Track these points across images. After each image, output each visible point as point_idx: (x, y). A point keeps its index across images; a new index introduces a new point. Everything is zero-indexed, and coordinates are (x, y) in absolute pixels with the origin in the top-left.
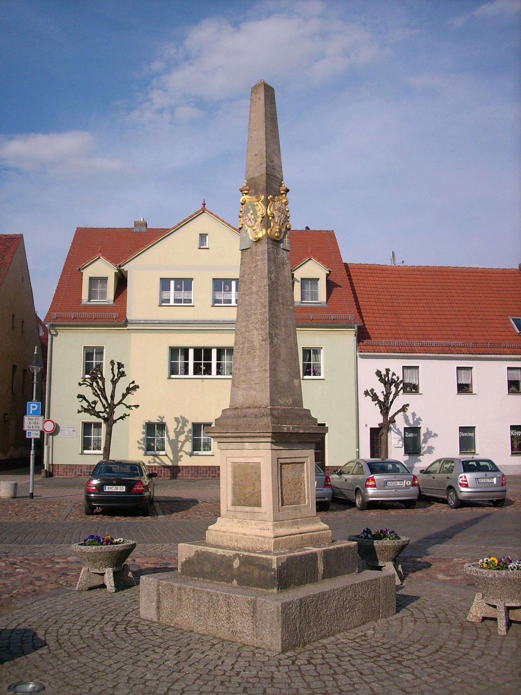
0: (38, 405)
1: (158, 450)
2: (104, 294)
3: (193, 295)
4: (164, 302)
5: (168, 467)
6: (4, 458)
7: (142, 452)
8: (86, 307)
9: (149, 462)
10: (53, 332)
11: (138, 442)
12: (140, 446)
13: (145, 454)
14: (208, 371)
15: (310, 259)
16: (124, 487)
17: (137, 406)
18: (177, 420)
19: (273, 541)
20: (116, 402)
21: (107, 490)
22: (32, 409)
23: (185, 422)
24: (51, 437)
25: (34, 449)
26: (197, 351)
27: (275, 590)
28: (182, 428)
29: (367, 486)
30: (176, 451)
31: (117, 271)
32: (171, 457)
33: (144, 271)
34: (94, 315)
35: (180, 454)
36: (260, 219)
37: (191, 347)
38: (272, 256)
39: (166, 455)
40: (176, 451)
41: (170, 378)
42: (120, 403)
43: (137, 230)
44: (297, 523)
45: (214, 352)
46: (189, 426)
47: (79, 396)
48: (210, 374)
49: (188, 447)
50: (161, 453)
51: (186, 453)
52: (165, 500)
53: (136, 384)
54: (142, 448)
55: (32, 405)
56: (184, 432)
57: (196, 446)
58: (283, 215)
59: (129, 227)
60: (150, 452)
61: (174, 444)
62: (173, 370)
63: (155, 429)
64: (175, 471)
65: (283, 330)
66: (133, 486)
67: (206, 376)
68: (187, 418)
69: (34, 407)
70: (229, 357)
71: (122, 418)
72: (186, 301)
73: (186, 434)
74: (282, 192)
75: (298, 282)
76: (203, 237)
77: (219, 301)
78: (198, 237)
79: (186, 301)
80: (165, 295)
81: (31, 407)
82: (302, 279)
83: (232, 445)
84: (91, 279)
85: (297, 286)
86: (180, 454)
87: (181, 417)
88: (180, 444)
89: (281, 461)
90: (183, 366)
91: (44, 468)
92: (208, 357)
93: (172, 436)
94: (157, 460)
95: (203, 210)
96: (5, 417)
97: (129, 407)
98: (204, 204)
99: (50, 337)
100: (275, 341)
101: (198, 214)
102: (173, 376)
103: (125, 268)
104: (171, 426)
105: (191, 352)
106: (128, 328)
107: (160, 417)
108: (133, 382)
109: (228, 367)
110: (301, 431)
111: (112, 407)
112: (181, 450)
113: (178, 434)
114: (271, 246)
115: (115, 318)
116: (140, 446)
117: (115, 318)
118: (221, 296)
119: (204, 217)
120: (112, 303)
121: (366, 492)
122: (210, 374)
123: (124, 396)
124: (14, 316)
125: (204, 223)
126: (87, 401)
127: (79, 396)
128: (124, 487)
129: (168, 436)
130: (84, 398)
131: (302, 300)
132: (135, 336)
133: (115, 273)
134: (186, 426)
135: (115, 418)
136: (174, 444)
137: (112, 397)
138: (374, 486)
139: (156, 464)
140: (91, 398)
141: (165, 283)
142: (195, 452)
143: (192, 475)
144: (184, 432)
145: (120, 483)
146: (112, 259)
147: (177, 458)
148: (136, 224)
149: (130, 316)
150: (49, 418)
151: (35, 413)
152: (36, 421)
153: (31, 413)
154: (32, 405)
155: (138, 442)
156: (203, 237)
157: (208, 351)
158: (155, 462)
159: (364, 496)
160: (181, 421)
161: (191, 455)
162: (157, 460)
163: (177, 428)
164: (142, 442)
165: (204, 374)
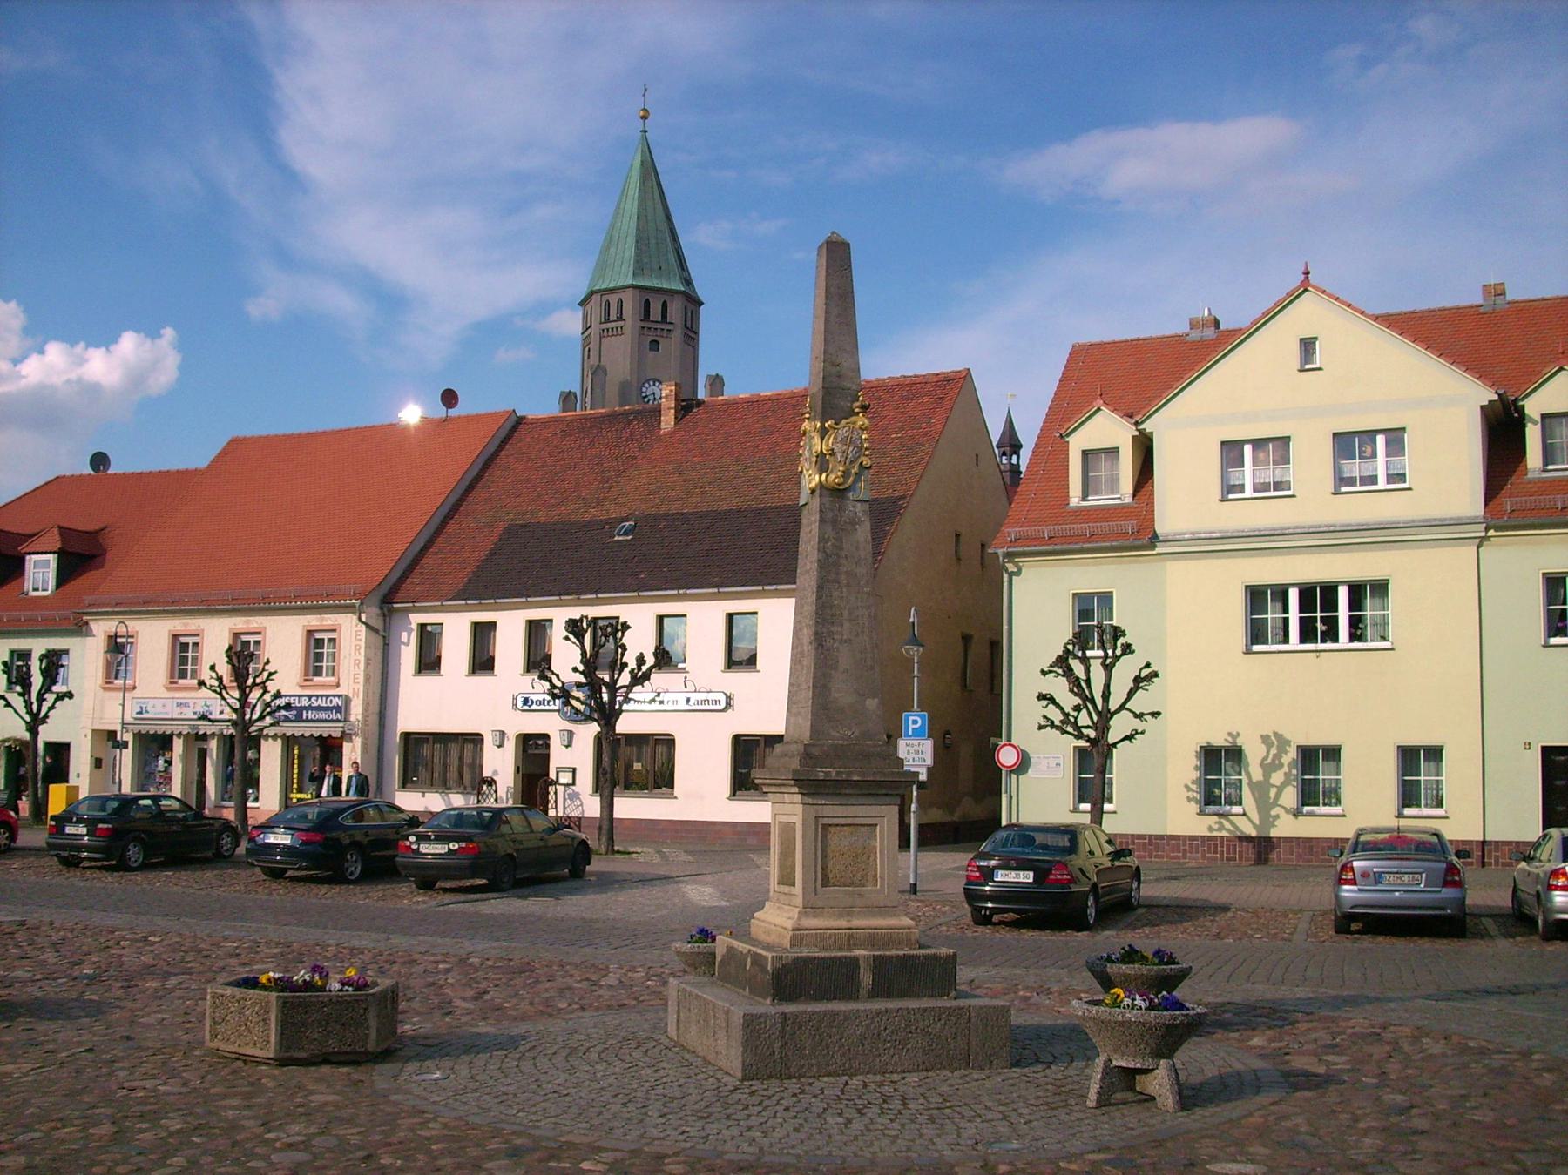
0: (922, 717)
1: (1231, 804)
2: (1114, 483)
3: (1292, 474)
4: (1230, 489)
5: (1249, 839)
6: (948, 819)
7: (1194, 807)
8: (1079, 511)
9: (1210, 829)
10: (1011, 567)
11: (1186, 786)
12: (1190, 794)
13: (1201, 813)
14: (1331, 634)
15: (1561, 369)
16: (1031, 874)
17: (1155, 714)
18: (1265, 739)
20: (1113, 706)
21: (999, 879)
22: (911, 726)
23: (1283, 743)
24: (1014, 777)
26: (1307, 593)
27: (769, 1001)
28: (1277, 756)
29: (1551, 888)
30: (1265, 805)
32: (1256, 818)
33: (1188, 428)
34: (1088, 528)
35: (1273, 813)
37: (1293, 585)
38: (830, 515)
39: (1244, 814)
40: (1265, 805)
41: (1248, 652)
42: (1122, 707)
43: (1195, 335)
44: (849, 914)
45: (1343, 594)
46: (1291, 754)
47: (1042, 697)
48: (1336, 640)
49: (1290, 797)
50: (1236, 809)
51: (1287, 811)
52: (1165, 902)
53: (1153, 668)
54: (1194, 799)
56: (1282, 765)
57: (1308, 795)
59: (1179, 332)
60: (1212, 808)
61: (1260, 789)
62: (1256, 634)
63: (1218, 761)
64: (1263, 847)
65: (847, 625)
66: (1049, 871)
67: (1329, 645)
68: (1287, 736)
69: (915, 722)
70: (1377, 601)
71: (1129, 738)
72: (1278, 486)
73: (1286, 769)
75: (1535, 423)
76: (1308, 346)
77: (1351, 481)
78: (1295, 348)
79: (1278, 486)
80: (1234, 473)
82: (1544, 416)
83: (852, 800)
84: (1085, 454)
85: (1533, 435)
86: (1273, 813)
87: (1275, 734)
88: (1273, 792)
89: (826, 821)
90: (1280, 624)
92: (1330, 603)
93: (1257, 773)
94: (1227, 825)
95: (1305, 287)
97: (1139, 716)
98: (1307, 273)
99: (1006, 577)
100: (828, 643)
101: (1294, 297)
102: (1256, 648)
103: (1148, 426)
104: (1254, 753)
105: (1293, 595)
106: (1157, 550)
107: (1230, 734)
108: (1148, 665)
109: (1374, 624)
111: (1105, 717)
112: (1275, 804)
113: (1269, 768)
114: (826, 500)
115: (1133, 531)
116: (1190, 794)
117: (1133, 531)
118: (1354, 468)
119: (1308, 302)
120: (1128, 500)
121: (1550, 900)
122: (1336, 640)
123: (1131, 694)
125: (1308, 315)
126: (1058, 706)
127: (1042, 697)
128: (1031, 874)
129: (1249, 775)
130: (1052, 700)
131: (1546, 463)
132: (1175, 568)
134: (1286, 752)
135: (1111, 740)
136: (1260, 789)
137: (1106, 696)
138: (1353, 882)
139: (1224, 833)
140: (1069, 700)
141: (1231, 451)
142: (1306, 809)
143: (1299, 857)
144: (1282, 765)
145: (1022, 866)
146: (1133, 412)
147: (1267, 820)
148: (1194, 324)
149: (1163, 526)
150: (1009, 739)
151: (917, 733)
155: (1186, 786)
156: (1308, 346)
157: (1329, 592)
158: (1222, 828)
159: (1548, 910)
160: (1275, 741)
161: (1297, 813)
162: (1227, 825)
163: (1265, 758)
164: (1194, 787)
165: (1323, 641)
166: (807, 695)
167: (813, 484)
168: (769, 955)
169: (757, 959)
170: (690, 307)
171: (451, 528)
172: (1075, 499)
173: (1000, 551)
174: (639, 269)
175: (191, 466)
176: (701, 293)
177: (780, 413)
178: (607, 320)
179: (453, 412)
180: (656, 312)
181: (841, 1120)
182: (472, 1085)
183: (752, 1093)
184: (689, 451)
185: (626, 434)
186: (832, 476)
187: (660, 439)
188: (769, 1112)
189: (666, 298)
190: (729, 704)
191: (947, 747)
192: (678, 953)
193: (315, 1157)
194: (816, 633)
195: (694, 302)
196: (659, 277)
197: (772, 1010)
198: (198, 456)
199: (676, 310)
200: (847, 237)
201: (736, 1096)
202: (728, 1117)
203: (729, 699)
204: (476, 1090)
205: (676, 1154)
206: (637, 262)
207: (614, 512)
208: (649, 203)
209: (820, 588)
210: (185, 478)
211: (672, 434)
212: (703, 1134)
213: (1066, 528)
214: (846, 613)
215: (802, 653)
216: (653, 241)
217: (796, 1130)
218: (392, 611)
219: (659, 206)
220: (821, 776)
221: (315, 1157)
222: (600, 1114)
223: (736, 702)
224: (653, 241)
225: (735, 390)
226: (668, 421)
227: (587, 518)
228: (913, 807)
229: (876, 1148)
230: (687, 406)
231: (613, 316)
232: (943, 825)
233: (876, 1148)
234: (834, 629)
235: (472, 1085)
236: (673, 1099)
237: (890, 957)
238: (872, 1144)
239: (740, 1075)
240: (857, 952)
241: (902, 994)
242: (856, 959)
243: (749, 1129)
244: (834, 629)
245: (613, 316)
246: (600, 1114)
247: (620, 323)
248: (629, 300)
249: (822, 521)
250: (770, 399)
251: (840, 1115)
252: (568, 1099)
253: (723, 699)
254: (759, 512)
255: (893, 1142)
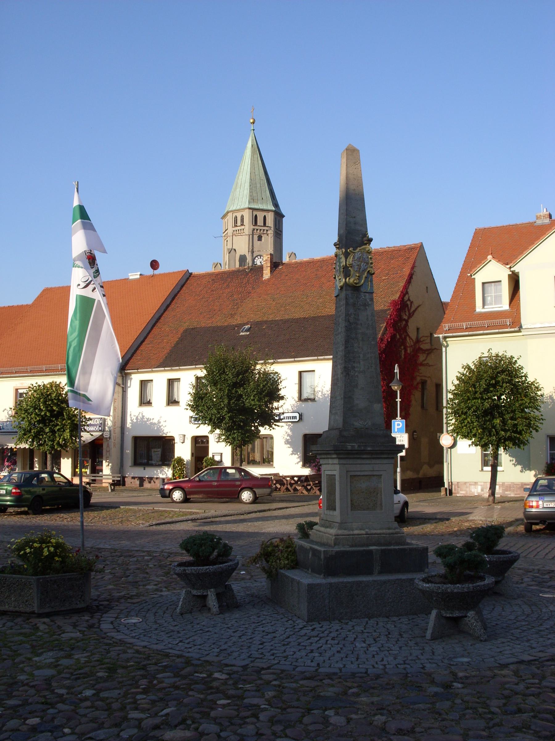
2: (498, 299)
6: (415, 476)
19: (334, 537)
22: (396, 427)
25: (401, 467)
27: (322, 576)
31: (511, 273)
36: (342, 270)
43: (539, 222)
55: (396, 423)
58: (363, 263)
65: (362, 363)
69: (398, 425)
74: (365, 242)
81: (396, 425)
91: (444, 486)
96: (413, 434)
103: (516, 269)
110: (369, 449)
114: (349, 292)
124: (418, 329)
133: (509, 275)
151: (399, 431)
152: (401, 439)
153: (396, 431)
154: (396, 423)
166: (340, 402)
167: (342, 284)
168: (322, 549)
169: (315, 551)
170: (278, 218)
171: (156, 330)
172: (479, 308)
173: (441, 336)
174: (252, 199)
175: (25, 303)
176: (283, 212)
177: (324, 268)
178: (236, 226)
179: (157, 272)
180: (260, 222)
181: (364, 645)
182: (155, 626)
183: (313, 630)
184: (278, 288)
185: (245, 281)
186: (351, 280)
187: (263, 282)
188: (323, 641)
189: (265, 214)
190: (301, 419)
191: (414, 439)
192: (178, 574)
193: (59, 673)
194: (345, 367)
195: (279, 216)
196: (262, 203)
197: (324, 581)
198: (28, 299)
199: (270, 218)
200: (357, 146)
201: (303, 632)
202: (299, 644)
203: (301, 415)
204: (156, 629)
205: (269, 668)
206: (250, 196)
207: (237, 320)
208: (256, 166)
209: (347, 342)
210: (21, 308)
211: (269, 280)
212: (285, 654)
213: (476, 323)
214: (361, 356)
215: (337, 379)
216: (258, 185)
217: (338, 652)
218: (127, 374)
219: (260, 162)
220: (349, 448)
221: (59, 673)
222: (226, 643)
223: (304, 417)
224: (258, 185)
225: (303, 256)
226: (267, 274)
227: (226, 324)
228: (399, 470)
229: (385, 662)
230: (275, 264)
231: (239, 223)
232: (413, 479)
233: (385, 662)
234: (356, 365)
235: (155, 626)
236: (268, 633)
237: (390, 550)
238: (382, 660)
239: (306, 619)
240: (371, 548)
241: (398, 571)
242: (371, 552)
243: (312, 651)
244: (356, 365)
245: (239, 223)
246: (226, 643)
247: (243, 227)
248: (247, 216)
249: (347, 304)
250: (318, 261)
251: (364, 642)
252: (208, 634)
253: (297, 415)
254: (314, 319)
255: (395, 659)
